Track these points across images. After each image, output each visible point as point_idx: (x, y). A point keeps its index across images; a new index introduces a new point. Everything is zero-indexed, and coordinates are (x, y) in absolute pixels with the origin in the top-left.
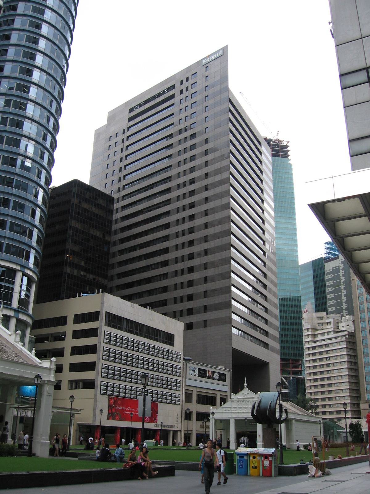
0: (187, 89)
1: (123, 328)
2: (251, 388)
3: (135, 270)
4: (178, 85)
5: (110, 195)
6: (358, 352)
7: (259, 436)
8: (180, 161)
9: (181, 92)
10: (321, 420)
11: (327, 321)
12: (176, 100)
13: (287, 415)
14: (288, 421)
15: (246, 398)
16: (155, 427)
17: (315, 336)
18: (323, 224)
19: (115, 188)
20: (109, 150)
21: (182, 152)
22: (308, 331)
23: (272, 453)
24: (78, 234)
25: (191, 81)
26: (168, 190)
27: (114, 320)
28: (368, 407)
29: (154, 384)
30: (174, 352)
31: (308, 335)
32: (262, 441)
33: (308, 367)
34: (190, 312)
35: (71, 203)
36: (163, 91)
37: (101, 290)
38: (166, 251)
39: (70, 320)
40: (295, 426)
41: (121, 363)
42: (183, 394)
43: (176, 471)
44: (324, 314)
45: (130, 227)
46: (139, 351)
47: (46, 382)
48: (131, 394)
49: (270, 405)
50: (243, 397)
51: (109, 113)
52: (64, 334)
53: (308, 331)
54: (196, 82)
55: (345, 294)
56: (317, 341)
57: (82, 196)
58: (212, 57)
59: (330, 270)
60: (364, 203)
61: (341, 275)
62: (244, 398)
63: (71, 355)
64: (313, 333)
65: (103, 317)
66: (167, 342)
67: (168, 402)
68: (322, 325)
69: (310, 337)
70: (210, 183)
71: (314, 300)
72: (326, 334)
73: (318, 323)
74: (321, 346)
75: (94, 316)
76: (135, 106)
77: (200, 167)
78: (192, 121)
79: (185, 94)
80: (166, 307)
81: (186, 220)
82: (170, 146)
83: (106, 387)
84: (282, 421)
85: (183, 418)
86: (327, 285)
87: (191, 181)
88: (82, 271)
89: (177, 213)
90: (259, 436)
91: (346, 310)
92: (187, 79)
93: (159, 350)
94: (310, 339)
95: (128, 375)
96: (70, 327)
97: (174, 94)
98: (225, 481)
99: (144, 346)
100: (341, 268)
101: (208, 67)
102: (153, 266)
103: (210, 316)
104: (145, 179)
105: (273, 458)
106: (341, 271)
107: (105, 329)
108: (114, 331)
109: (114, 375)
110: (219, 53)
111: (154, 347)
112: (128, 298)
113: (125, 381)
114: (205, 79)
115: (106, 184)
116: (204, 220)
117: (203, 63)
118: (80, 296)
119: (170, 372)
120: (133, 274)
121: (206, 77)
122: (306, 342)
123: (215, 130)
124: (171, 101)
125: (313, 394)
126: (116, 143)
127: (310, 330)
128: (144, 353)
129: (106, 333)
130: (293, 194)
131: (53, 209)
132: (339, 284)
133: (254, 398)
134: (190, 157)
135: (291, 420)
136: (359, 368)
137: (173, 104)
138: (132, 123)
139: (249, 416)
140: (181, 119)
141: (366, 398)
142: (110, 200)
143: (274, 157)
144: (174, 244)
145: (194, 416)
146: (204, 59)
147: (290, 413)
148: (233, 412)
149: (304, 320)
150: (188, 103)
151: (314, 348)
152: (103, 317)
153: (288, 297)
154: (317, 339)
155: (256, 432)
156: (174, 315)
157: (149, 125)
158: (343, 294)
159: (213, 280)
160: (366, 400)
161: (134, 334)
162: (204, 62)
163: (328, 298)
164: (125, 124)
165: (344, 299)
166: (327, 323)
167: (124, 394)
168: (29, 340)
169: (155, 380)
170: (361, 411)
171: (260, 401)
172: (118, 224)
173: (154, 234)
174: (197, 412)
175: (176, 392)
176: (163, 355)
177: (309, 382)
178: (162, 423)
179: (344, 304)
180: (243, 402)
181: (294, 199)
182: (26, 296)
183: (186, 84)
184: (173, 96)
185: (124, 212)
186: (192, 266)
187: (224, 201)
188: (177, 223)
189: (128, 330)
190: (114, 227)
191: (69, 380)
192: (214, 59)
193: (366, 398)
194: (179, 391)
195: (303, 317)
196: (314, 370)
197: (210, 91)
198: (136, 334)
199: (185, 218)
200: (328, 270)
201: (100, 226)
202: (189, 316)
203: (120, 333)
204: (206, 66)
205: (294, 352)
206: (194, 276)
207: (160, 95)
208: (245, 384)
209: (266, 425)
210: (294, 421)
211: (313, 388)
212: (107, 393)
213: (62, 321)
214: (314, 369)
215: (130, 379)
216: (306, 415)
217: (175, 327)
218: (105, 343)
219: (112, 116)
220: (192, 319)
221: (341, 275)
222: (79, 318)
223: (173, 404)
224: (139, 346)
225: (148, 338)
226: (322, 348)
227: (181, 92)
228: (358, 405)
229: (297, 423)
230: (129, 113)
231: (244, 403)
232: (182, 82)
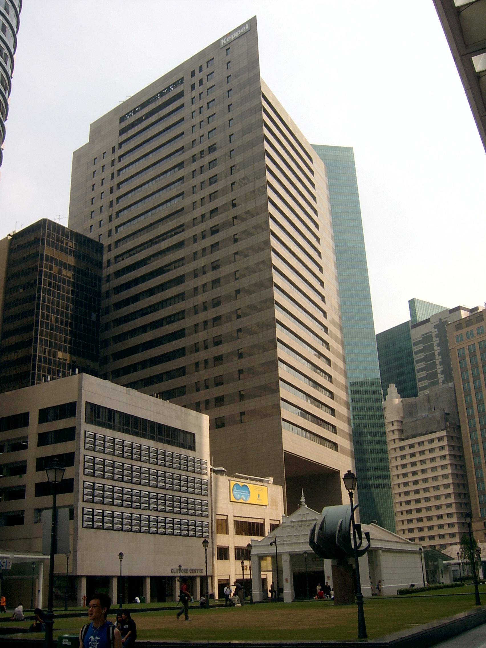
0: (201, 82)
1: (114, 426)
2: (311, 504)
3: (166, 283)
4: (188, 78)
5: (97, 240)
6: (473, 508)
7: (328, 577)
8: (196, 202)
9: (193, 87)
10: (422, 548)
12: (186, 99)
13: (369, 541)
14: (372, 552)
15: (305, 521)
16: (172, 572)
18: (459, 59)
19: (104, 230)
20: (94, 177)
21: (199, 204)
23: (2, 147)
24: (64, 245)
25: (206, 71)
26: (181, 245)
27: (99, 415)
28: (483, 528)
29: (168, 509)
30: (196, 460)
32: (291, 588)
33: (398, 502)
34: (220, 401)
35: (72, 363)
36: (167, 88)
37: (77, 370)
39: (34, 418)
40: (385, 560)
41: (113, 479)
42: (212, 521)
43: (477, 70)
45: (128, 285)
46: (141, 459)
47: (436, 563)
48: (157, 528)
49: (341, 526)
50: (300, 519)
51: (91, 125)
52: (26, 439)
54: (214, 72)
55: (440, 362)
57: (80, 275)
58: (235, 34)
60: (472, 52)
61: (435, 344)
62: (301, 521)
63: (36, 496)
65: (82, 410)
66: (129, 430)
67: (115, 528)
70: (220, 204)
75: (68, 410)
76: (129, 113)
77: (224, 191)
78: (210, 127)
79: (199, 89)
80: (184, 396)
81: (200, 366)
82: (181, 165)
83: (101, 518)
84: (362, 553)
85: (435, 324)
86: (420, 386)
87: (215, 301)
88: (60, 350)
89: (194, 243)
90: (287, 580)
91: (438, 347)
92: (201, 69)
93: (173, 463)
95: (134, 498)
96: (34, 429)
97: (183, 91)
98: (451, 374)
99: (149, 452)
100: (434, 335)
101: (229, 48)
102: (153, 308)
103: (249, 405)
104: (139, 234)
105: (181, 605)
106: (434, 339)
107: (87, 429)
108: (101, 431)
109: (113, 498)
110: (244, 28)
111: (179, 457)
112: (167, 396)
113: (122, 506)
114: (226, 53)
115: (100, 236)
116: (233, 248)
117: (222, 44)
118: (47, 381)
119: (191, 512)
120: (136, 353)
121: (227, 63)
123: (244, 137)
124: (178, 101)
125: (401, 477)
126: (103, 167)
127: (395, 424)
128: (149, 463)
129: (88, 433)
131: (11, 296)
132: (432, 357)
133: (317, 520)
134: (210, 179)
135: (281, 555)
136: (468, 473)
137: (182, 106)
138: (124, 137)
139: (308, 548)
140: (195, 126)
141: (353, 543)
142: (98, 247)
143: (186, 335)
144: (191, 305)
145: (232, 554)
146: (223, 38)
147: (373, 539)
148: (287, 544)
150: (203, 102)
152: (82, 410)
153: (361, 380)
155: (323, 572)
156: (198, 407)
157: (148, 137)
158: (439, 371)
159: (253, 396)
160: (480, 516)
161: (140, 418)
162: (223, 42)
164: (115, 139)
165: (438, 359)
167: (121, 526)
168: (158, 602)
169: (168, 503)
170: (474, 533)
171: (323, 521)
172: (111, 282)
173: (163, 293)
175: (203, 519)
176: (180, 464)
178: (180, 566)
179: (438, 366)
180: (301, 526)
182: (381, 407)
183: (199, 76)
184: (181, 95)
185: (118, 248)
186: (214, 271)
187: (261, 238)
188: (206, 407)
189: (132, 431)
190: (105, 287)
191: (35, 509)
192: (238, 37)
193: (353, 543)
194: (207, 516)
197: (234, 82)
198: (136, 434)
199: (207, 321)
200: (416, 339)
201: (92, 328)
202: (218, 409)
203: (109, 433)
204: (227, 47)
205: (381, 489)
206: (224, 349)
207: (162, 94)
208: (303, 499)
209: (336, 561)
210: (380, 551)
212: (93, 525)
213: (22, 420)
215: (130, 503)
216: (404, 543)
217: (201, 424)
218: (87, 449)
219: (97, 129)
220: (225, 411)
221: (440, 381)
222: (45, 415)
223: (198, 537)
224: (165, 480)
225: (154, 440)
227: (193, 87)
228: (469, 525)
229: (386, 554)
230: (120, 123)
231: (302, 529)
232: (193, 74)
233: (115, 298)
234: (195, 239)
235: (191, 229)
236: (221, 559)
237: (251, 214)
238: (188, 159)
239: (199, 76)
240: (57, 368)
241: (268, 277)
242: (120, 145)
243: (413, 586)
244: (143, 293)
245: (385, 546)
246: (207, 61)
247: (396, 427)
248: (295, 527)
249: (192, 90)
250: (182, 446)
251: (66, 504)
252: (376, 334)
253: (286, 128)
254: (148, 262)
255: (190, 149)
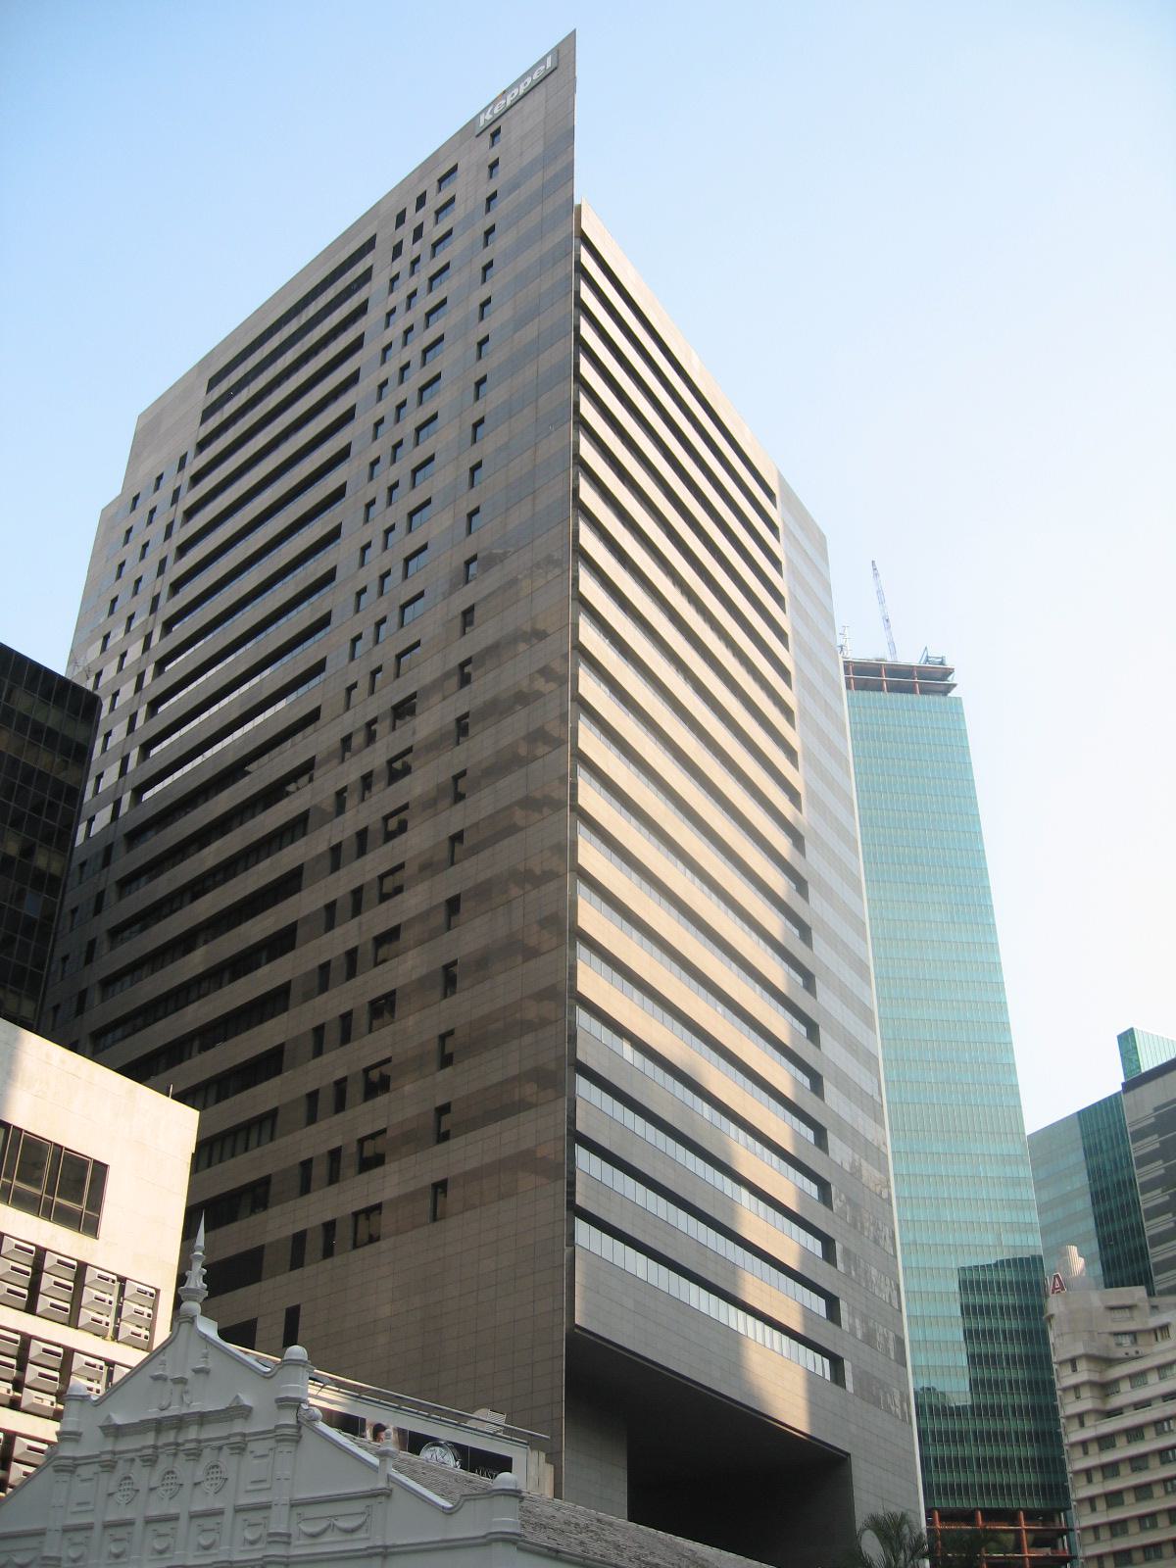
11: (1155, 1321)
15: (180, 1422)
17: (1106, 1388)
22: (1074, 1370)
31: (1076, 1388)
38: (290, 884)
44: (1139, 1293)
53: (1074, 1370)
56: (1117, 1412)
59: (1147, 1118)
64: (1096, 1377)
68: (1135, 1341)
69: (1085, 1393)
71: (1088, 1198)
72: (1153, 1378)
73: (1116, 1334)
74: (1135, 1433)
92: (421, 201)
94: (1087, 1403)
103: (464, 1154)
122: (1068, 1418)
130: (1005, 1027)
138: (358, 269)
149: (1053, 1322)
151: (1106, 1441)
154: (1116, 1402)
163: (1153, 1260)
166: (1154, 1331)
174: (145, 1517)
177: (1083, 1479)
181: (1009, 1030)
192: (525, 95)
195: (1051, 1313)
196: (1111, 1511)
200: (1137, 1122)
211: (1097, 1477)
214: (1114, 1535)
226: (1142, 1438)
233: (114, 958)
234: (323, 977)
235: (322, 883)
236: (1034, 1258)
237: (499, 1107)
238: (319, 858)
239: (413, 218)
240: (12, 804)
241: (185, 1243)
242: (202, 446)
243: (1127, 1354)
244: (1127, 1406)
245: (670, 1538)
246: (398, 651)
247: (1017, 1237)
248: (208, 1457)
249: (393, 259)
250: (66, 1218)
251: (35, 1243)
252: (1028, 1132)
253: (710, 416)
254: (291, 787)
255: (308, 997)
